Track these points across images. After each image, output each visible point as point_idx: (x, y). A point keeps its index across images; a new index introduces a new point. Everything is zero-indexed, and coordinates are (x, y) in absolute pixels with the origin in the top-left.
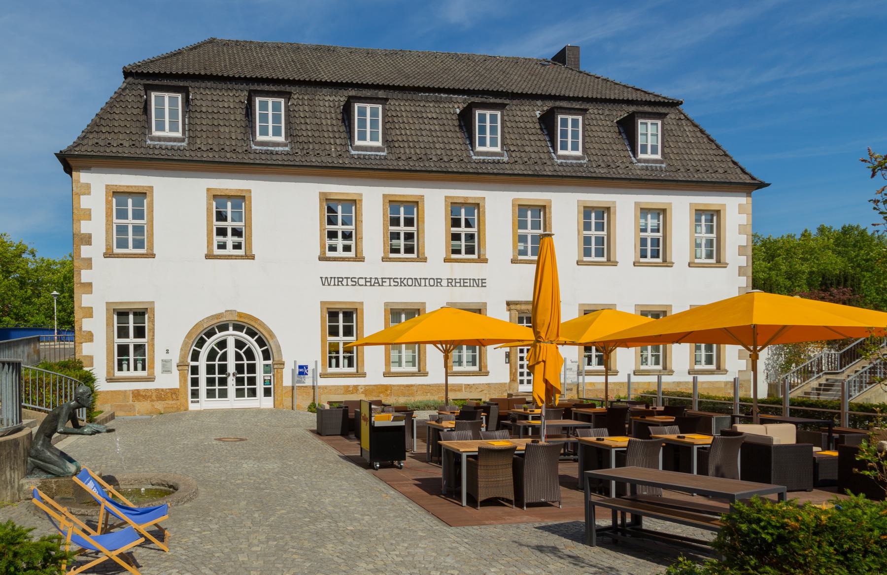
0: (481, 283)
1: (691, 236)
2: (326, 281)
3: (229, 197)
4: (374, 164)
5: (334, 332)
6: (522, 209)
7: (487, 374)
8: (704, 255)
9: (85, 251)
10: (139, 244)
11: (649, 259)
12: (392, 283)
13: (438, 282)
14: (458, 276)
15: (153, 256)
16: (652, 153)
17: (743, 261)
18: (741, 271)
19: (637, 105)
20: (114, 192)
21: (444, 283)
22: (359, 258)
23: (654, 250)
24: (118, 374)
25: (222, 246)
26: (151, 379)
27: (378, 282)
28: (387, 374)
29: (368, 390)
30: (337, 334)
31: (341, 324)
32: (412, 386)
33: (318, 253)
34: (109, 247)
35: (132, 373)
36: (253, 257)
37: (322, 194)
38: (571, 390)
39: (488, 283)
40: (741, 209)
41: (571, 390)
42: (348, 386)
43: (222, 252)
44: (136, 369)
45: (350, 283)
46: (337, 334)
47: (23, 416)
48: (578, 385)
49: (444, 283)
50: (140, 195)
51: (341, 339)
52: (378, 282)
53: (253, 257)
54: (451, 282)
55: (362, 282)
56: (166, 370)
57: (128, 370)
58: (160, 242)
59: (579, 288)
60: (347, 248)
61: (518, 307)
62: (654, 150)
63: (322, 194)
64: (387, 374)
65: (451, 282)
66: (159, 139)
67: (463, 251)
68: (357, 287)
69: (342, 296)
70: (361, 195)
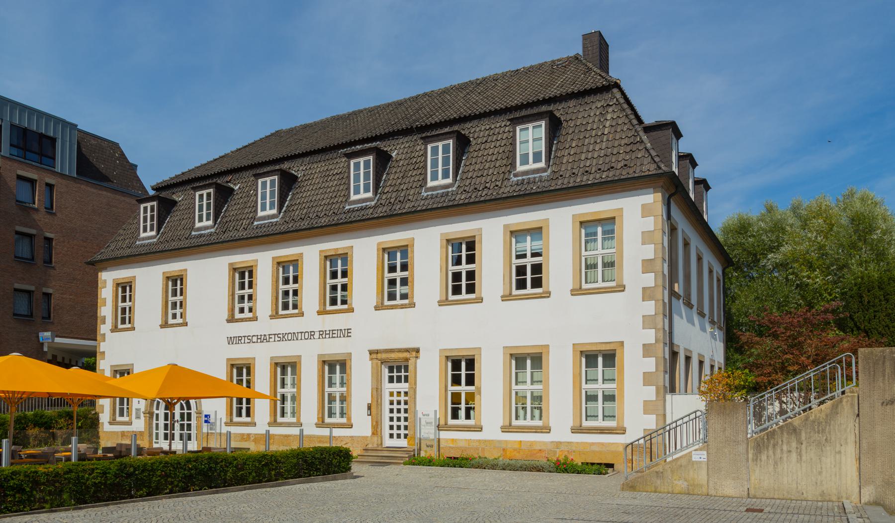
0: (346, 333)
1: (185, 299)
2: (231, 340)
3: (600, 221)
4: (271, 230)
5: (456, 380)
6: (586, 224)
8: (600, 279)
9: (650, 280)
11: (529, 290)
12: (277, 339)
13: (312, 334)
14: (327, 328)
17: (650, 280)
18: (647, 295)
19: (516, 111)
20: (581, 223)
23: (529, 277)
24: (119, 419)
26: (129, 423)
27: (263, 339)
28: (578, 429)
29: (257, 438)
30: (459, 384)
32: (289, 436)
33: (226, 315)
35: (529, 422)
37: (506, 227)
38: (432, 446)
39: (353, 333)
40: (646, 211)
41: (432, 446)
42: (243, 435)
43: (242, 316)
44: (533, 417)
45: (247, 341)
46: (459, 384)
48: (439, 440)
49: (317, 335)
51: (463, 388)
54: (323, 334)
55: (255, 339)
56: (138, 417)
57: (525, 419)
61: (379, 356)
62: (537, 157)
63: (506, 227)
64: (507, 428)
65: (323, 334)
66: (263, 218)
68: (251, 344)
69: (241, 352)
70: (186, 270)
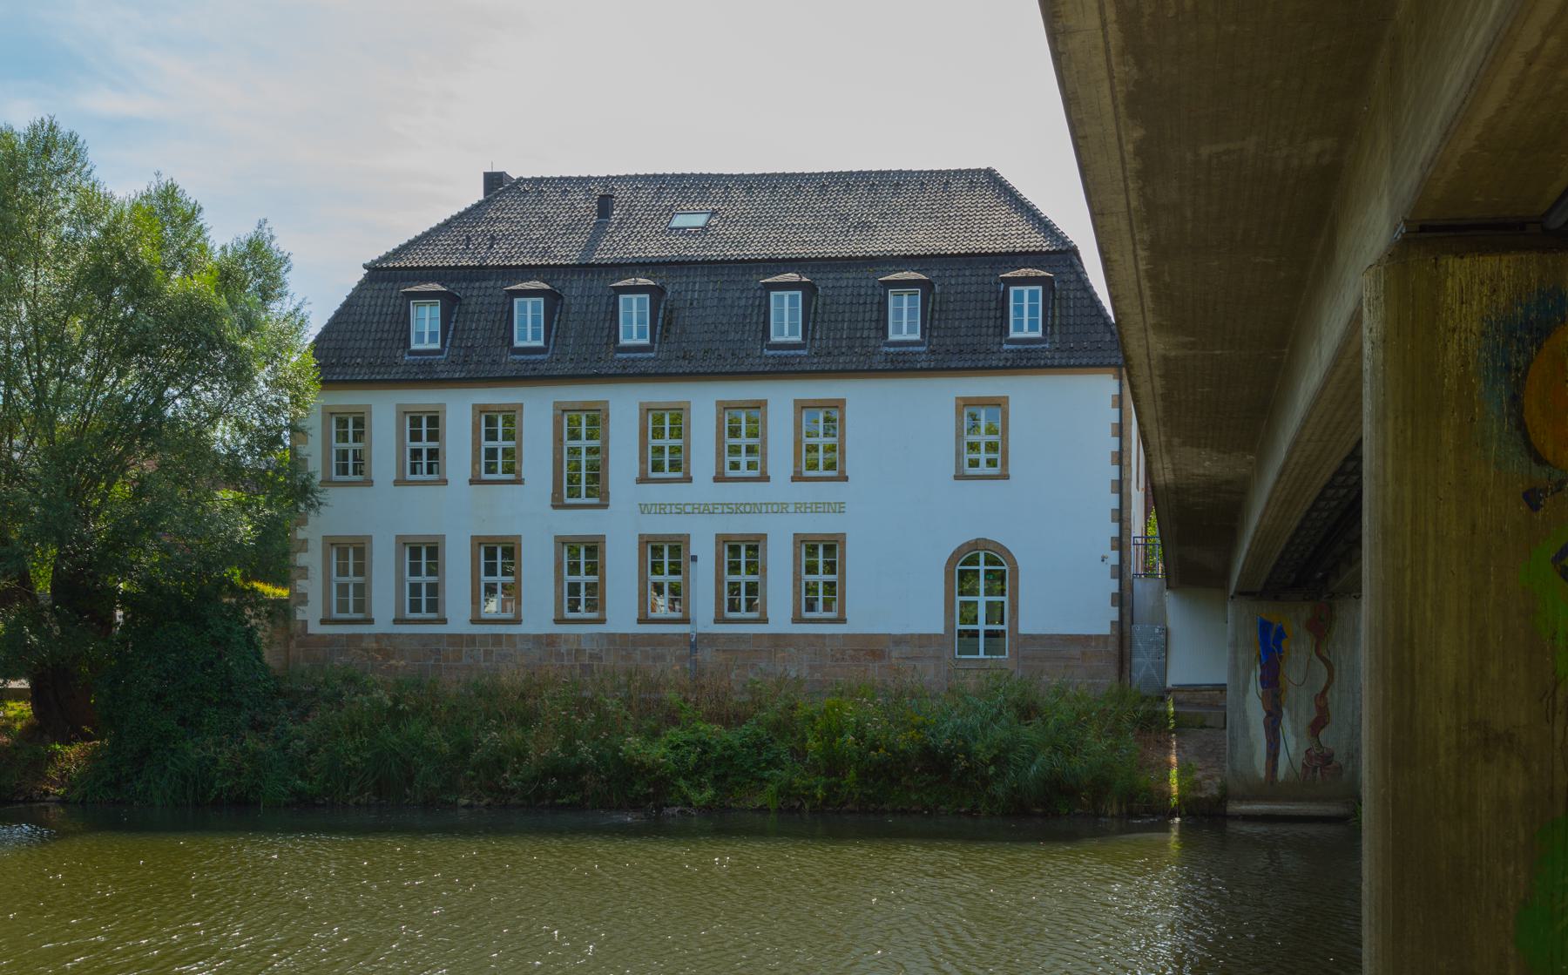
6: (967, 405)
7: (766, 621)
10: (509, 469)
15: (445, 482)
16: (1030, 330)
21: (791, 509)
22: (764, 478)
25: (735, 466)
27: (782, 508)
31: (821, 560)
34: (643, 472)
36: (846, 479)
47: (1113, 648)
50: (999, 403)
52: (707, 510)
53: (846, 479)
58: (853, 463)
59: (530, 513)
60: (750, 466)
67: (667, 467)
68: (682, 516)
